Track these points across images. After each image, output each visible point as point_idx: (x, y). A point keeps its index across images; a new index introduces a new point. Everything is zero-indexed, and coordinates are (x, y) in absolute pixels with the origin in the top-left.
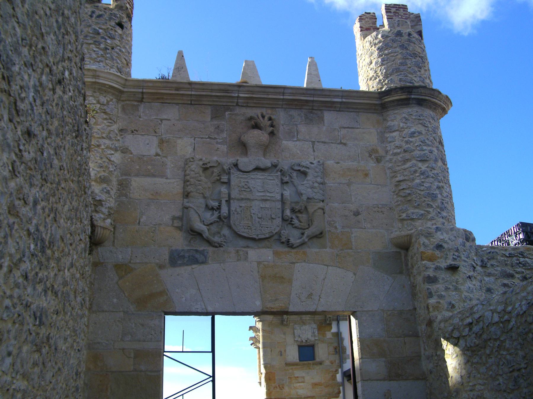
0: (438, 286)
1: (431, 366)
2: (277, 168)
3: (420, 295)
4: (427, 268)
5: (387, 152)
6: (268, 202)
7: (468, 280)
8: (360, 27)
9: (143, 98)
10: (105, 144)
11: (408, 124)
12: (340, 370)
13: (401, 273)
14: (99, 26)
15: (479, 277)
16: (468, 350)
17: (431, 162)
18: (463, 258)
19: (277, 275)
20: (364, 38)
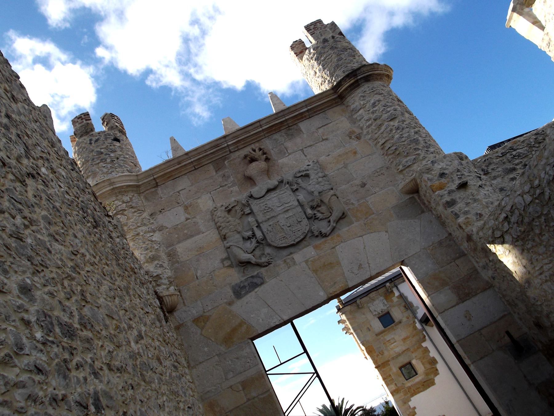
0: (459, 205)
1: (490, 273)
2: (284, 182)
3: (448, 221)
4: (442, 196)
5: (362, 129)
6: (290, 211)
7: (480, 189)
8: (295, 53)
9: (157, 183)
10: (142, 230)
11: (367, 99)
12: (416, 320)
13: (423, 212)
14: (99, 148)
15: (488, 183)
16: (517, 241)
17: (399, 113)
18: (466, 174)
19: (326, 264)
20: (302, 60)
